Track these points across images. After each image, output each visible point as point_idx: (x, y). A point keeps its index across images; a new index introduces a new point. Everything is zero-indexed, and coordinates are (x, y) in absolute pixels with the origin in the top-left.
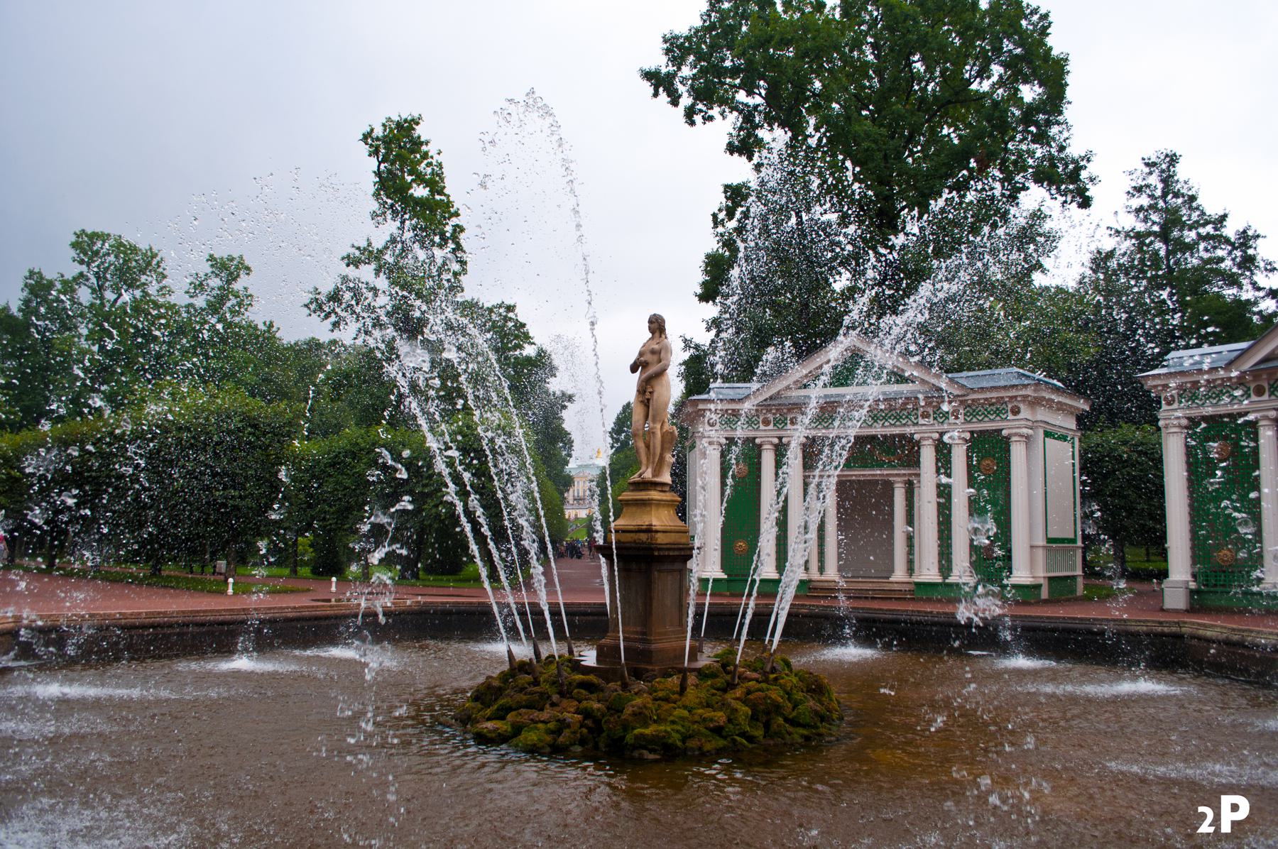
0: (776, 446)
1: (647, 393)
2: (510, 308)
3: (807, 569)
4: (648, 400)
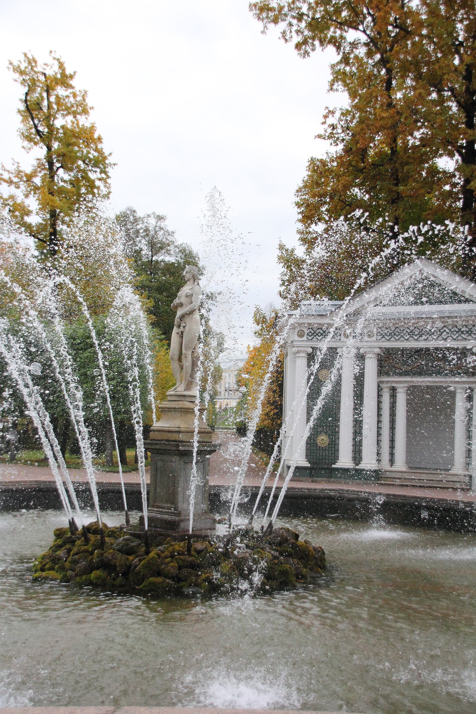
0: (309, 355)
1: (181, 327)
2: (160, 218)
3: (379, 461)
4: (182, 333)
